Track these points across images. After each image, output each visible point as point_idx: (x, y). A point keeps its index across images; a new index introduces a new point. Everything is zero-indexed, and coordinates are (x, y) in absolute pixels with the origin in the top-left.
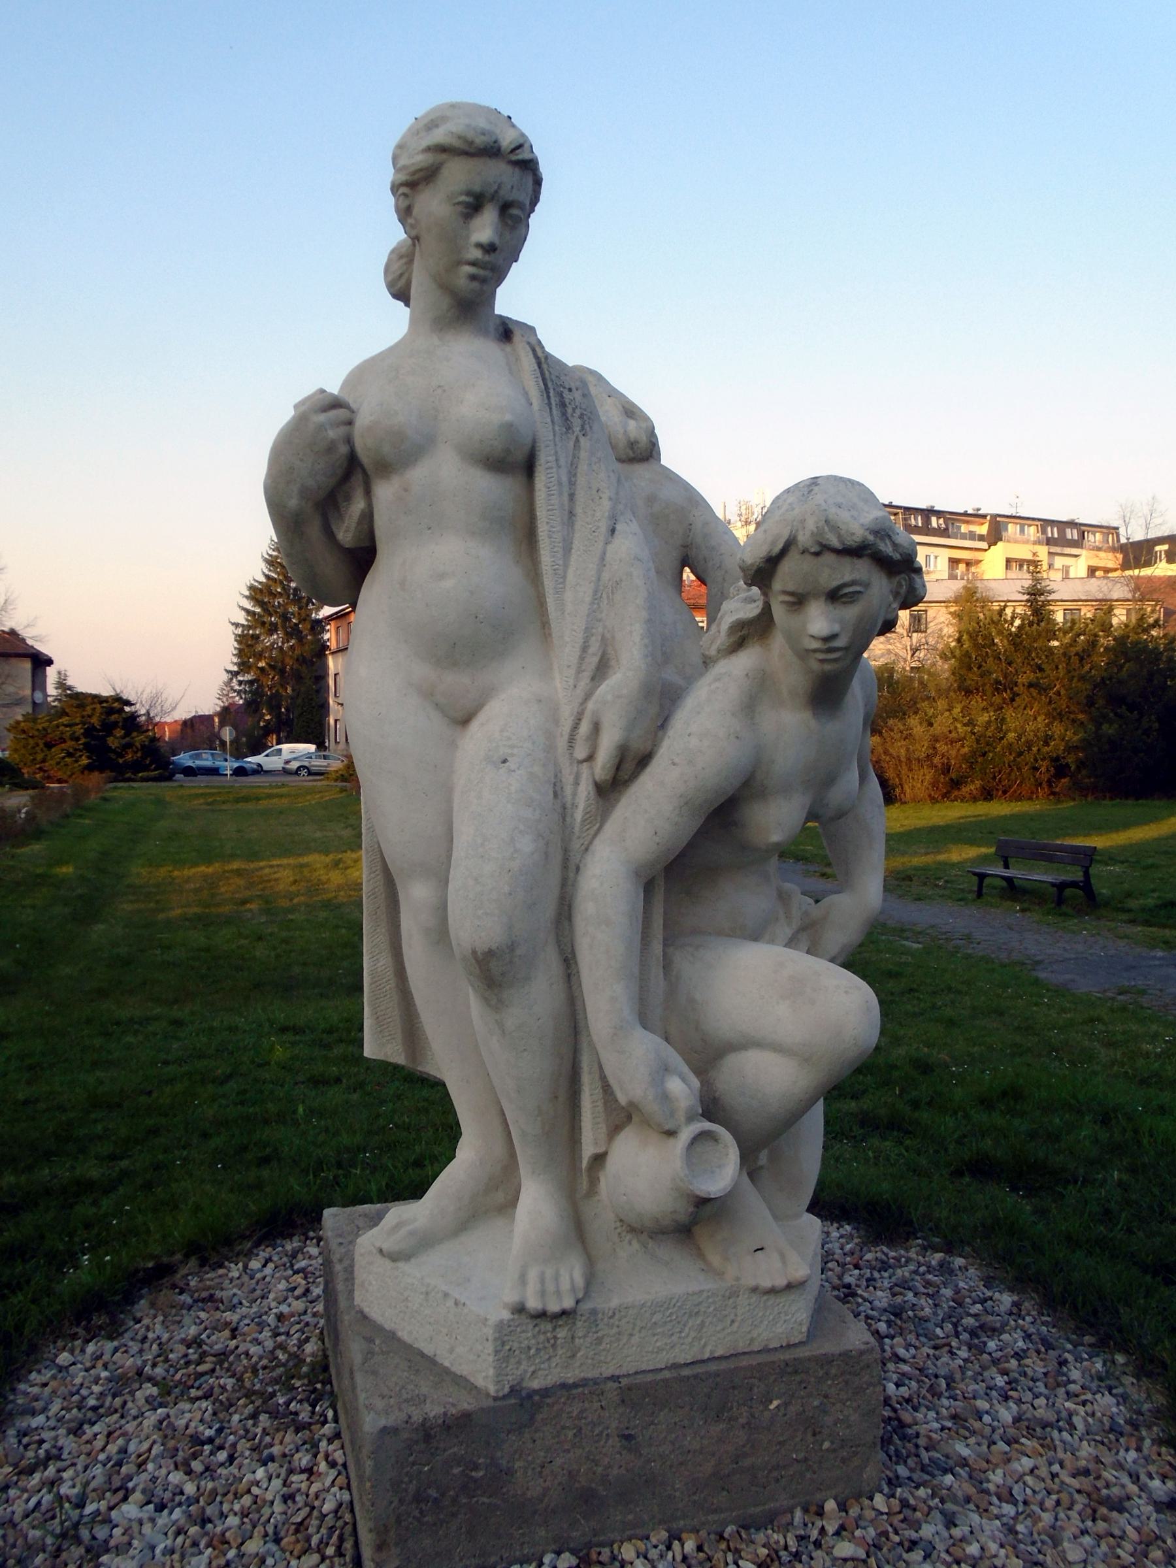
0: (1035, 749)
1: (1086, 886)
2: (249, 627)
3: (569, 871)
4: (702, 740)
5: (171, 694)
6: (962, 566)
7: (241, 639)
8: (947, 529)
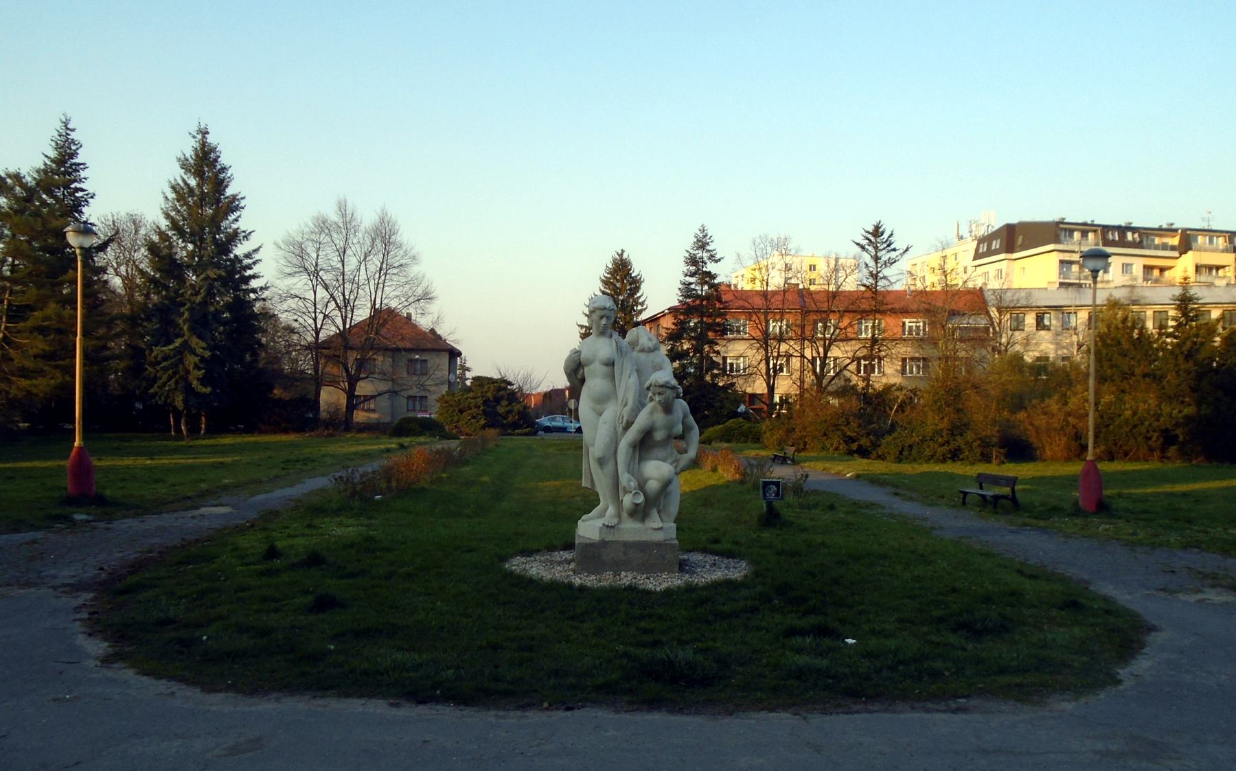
0: (1147, 423)
1: (1013, 499)
3: (617, 444)
4: (642, 420)
5: (537, 376)
6: (1156, 273)
8: (1141, 242)
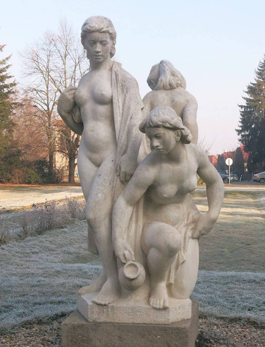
2: (247, 107)
7: (244, 114)
